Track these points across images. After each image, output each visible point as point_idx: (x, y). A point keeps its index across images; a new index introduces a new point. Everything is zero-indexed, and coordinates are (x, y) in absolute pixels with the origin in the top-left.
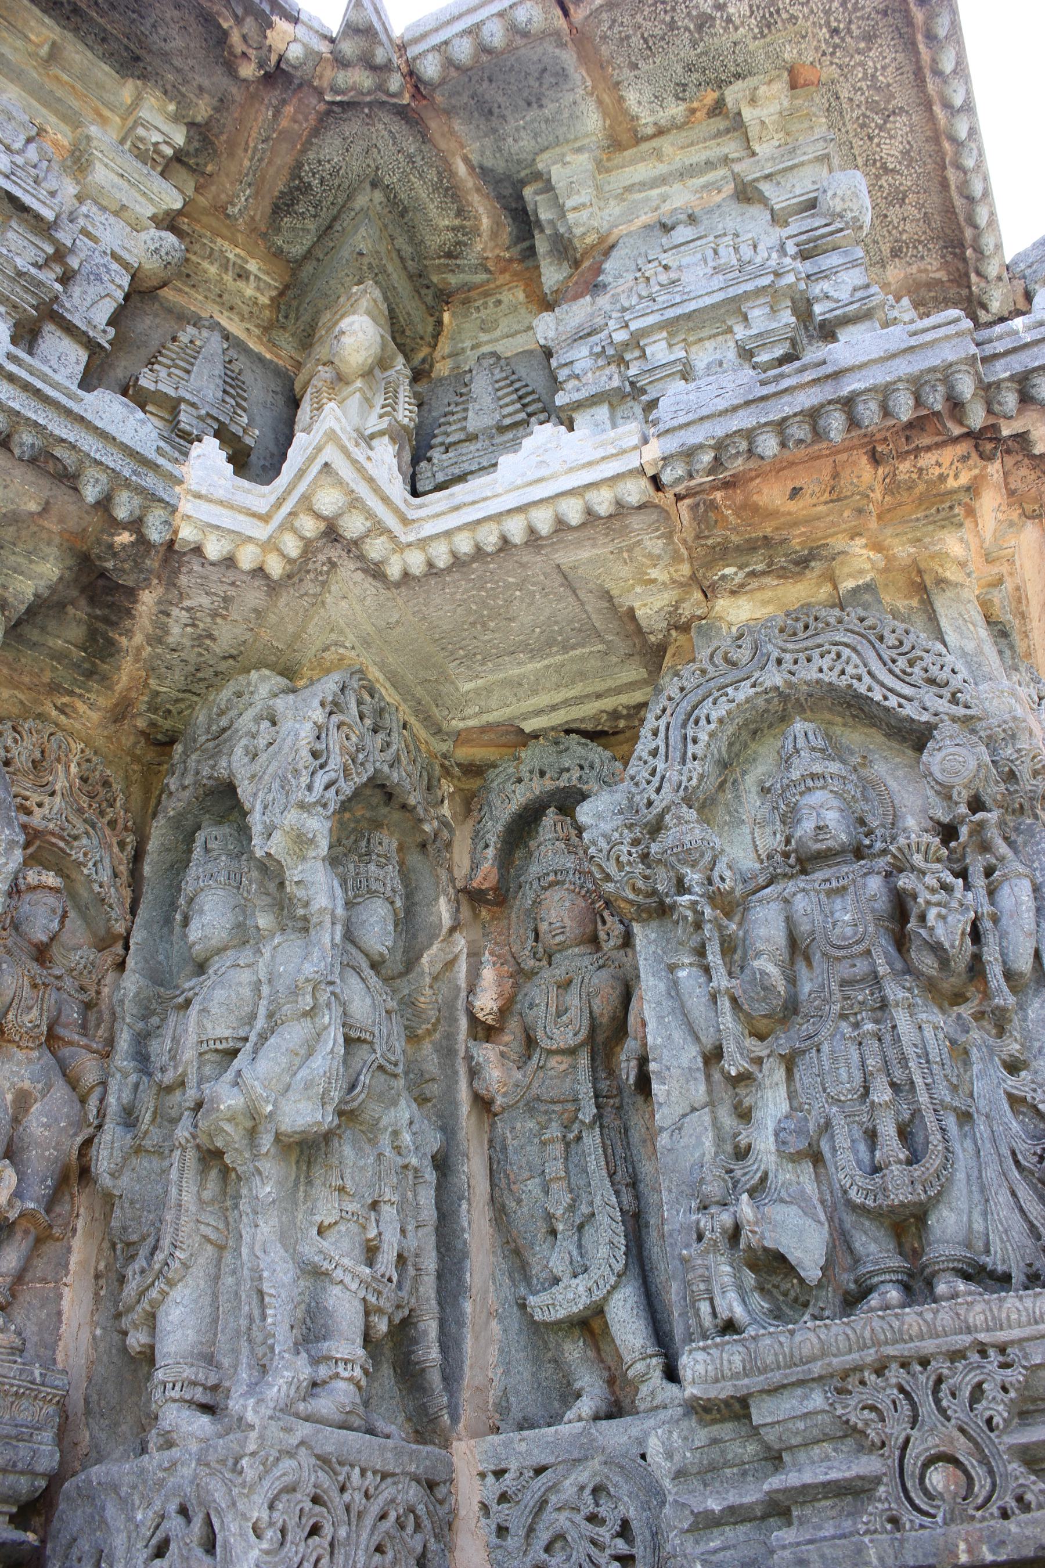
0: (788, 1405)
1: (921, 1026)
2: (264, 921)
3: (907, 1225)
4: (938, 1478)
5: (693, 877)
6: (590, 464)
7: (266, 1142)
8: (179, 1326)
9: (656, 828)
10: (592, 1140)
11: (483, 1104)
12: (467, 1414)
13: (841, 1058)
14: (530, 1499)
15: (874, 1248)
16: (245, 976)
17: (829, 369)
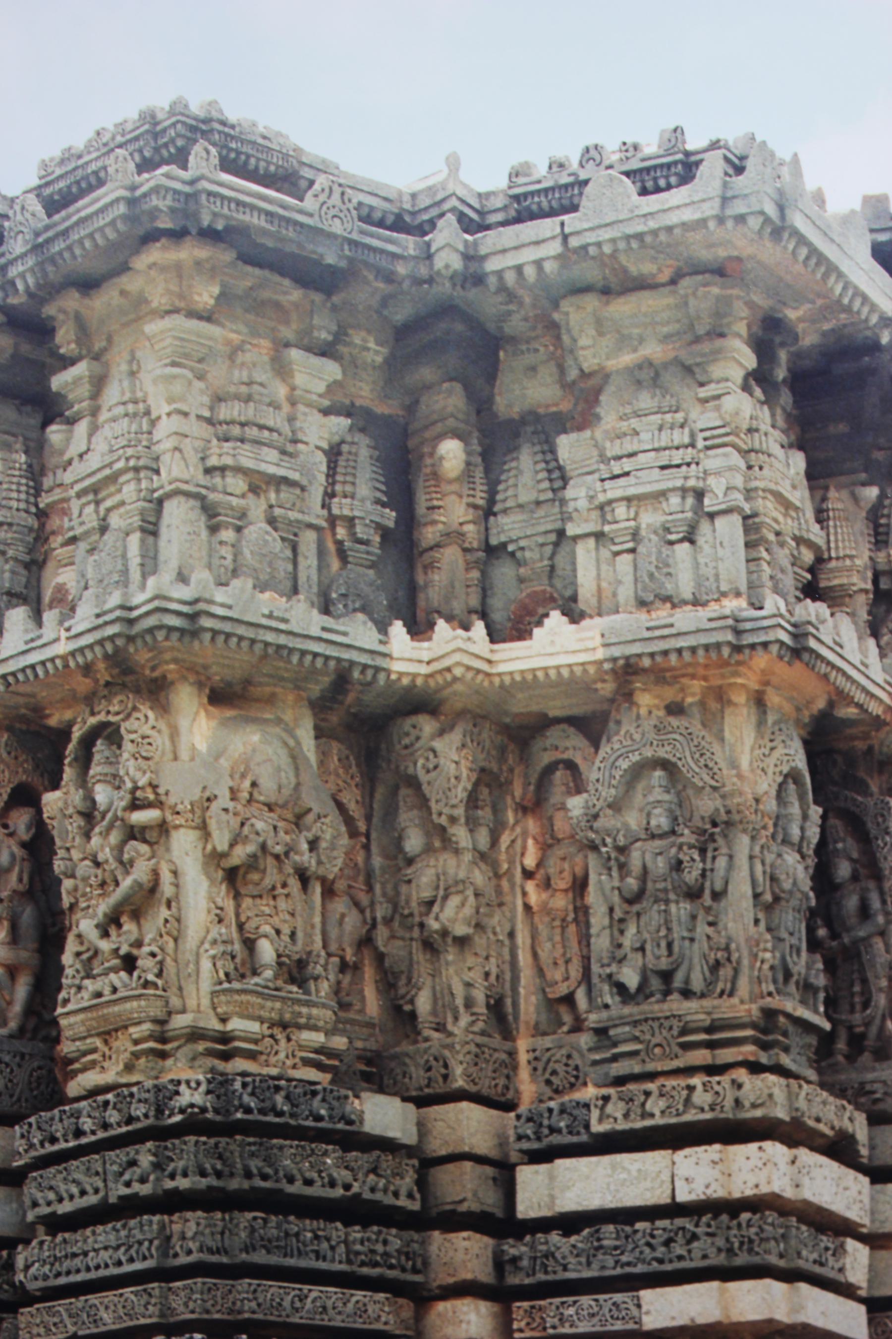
0: (619, 1030)
1: (681, 909)
2: (437, 844)
3: (666, 976)
4: (657, 1050)
5: (609, 840)
6: (574, 652)
7: (449, 940)
8: (423, 1003)
9: (596, 816)
10: (572, 928)
11: (527, 907)
12: (522, 1028)
13: (653, 916)
14: (544, 1059)
15: (655, 983)
16: (432, 871)
17: (673, 631)
